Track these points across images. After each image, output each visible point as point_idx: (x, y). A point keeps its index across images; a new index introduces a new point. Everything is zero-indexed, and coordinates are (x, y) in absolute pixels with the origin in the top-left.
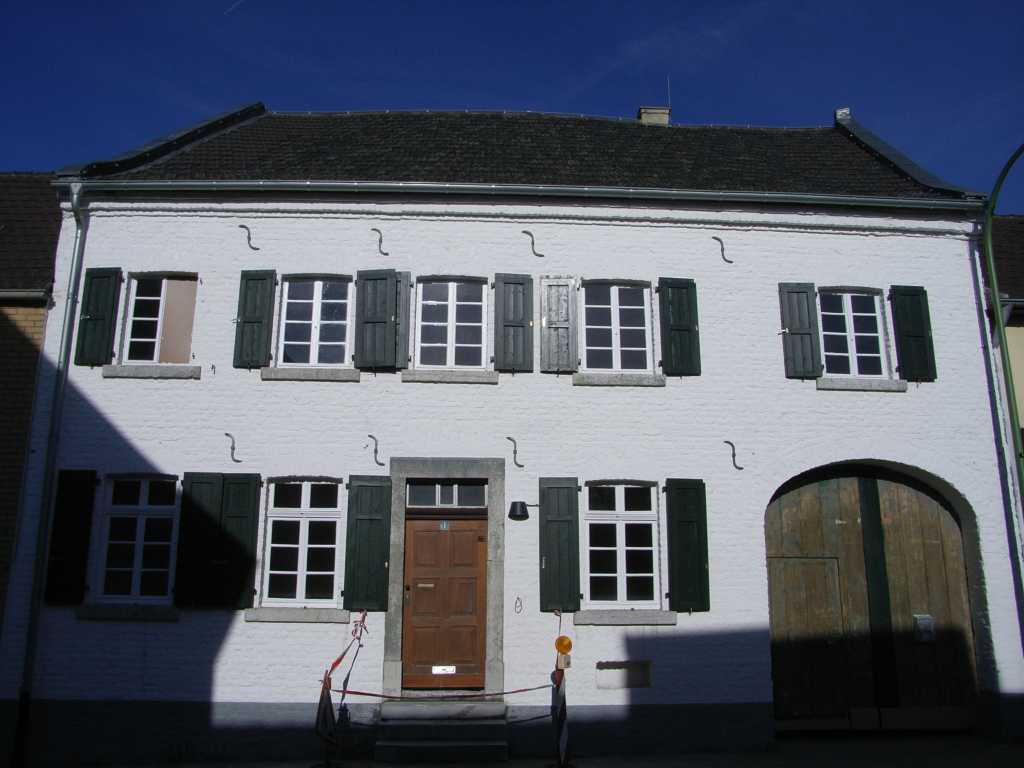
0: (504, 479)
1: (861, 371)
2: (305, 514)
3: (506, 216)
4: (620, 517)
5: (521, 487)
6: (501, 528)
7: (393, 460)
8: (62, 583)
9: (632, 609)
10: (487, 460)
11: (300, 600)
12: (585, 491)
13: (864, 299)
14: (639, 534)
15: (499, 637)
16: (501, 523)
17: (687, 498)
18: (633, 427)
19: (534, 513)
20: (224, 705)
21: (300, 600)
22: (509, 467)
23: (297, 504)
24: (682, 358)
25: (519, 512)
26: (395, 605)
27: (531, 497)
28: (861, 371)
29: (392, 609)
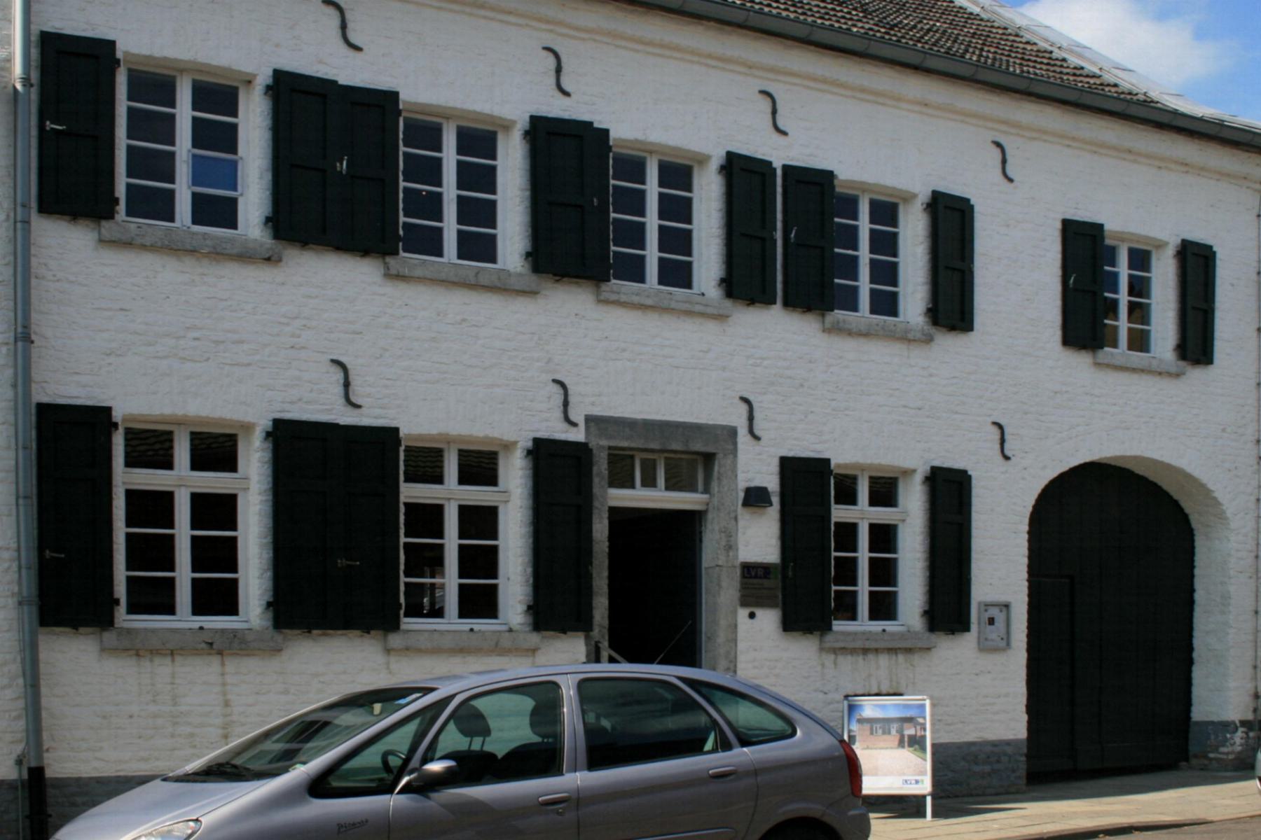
0: (735, 456)
1: (873, 311)
2: (863, 514)
3: (744, 64)
4: (183, 481)
5: (757, 466)
6: (733, 522)
7: (589, 419)
8: (69, 592)
9: (201, 628)
10: (715, 427)
11: (184, 619)
12: (121, 431)
13: (218, 96)
14: (217, 511)
15: (732, 666)
16: (733, 515)
17: (950, 492)
18: (891, 396)
19: (776, 500)
20: (51, 779)
21: (184, 619)
22: (743, 436)
23: (438, 479)
24: (953, 307)
25: (755, 498)
26: (600, 626)
27: (771, 482)
28: (873, 311)
29: (596, 633)
